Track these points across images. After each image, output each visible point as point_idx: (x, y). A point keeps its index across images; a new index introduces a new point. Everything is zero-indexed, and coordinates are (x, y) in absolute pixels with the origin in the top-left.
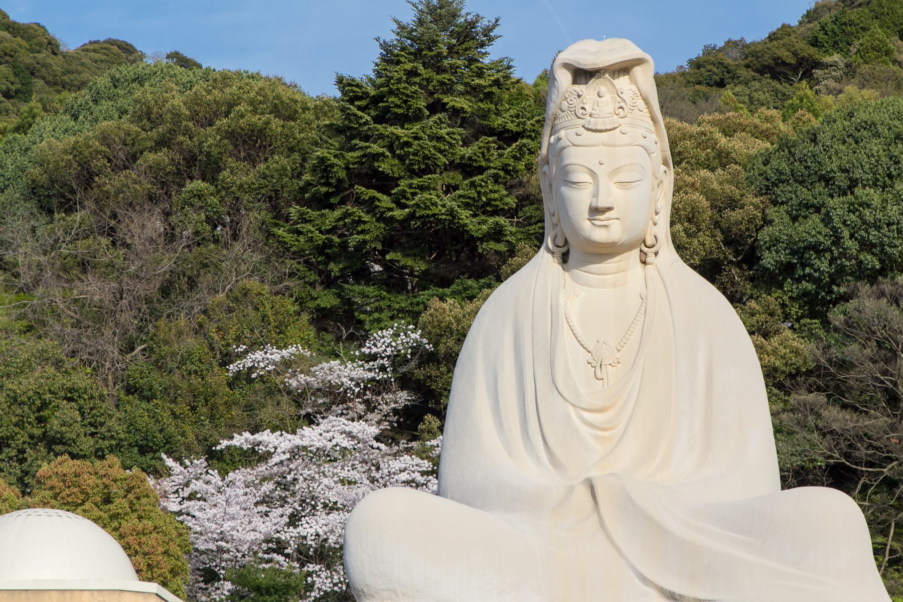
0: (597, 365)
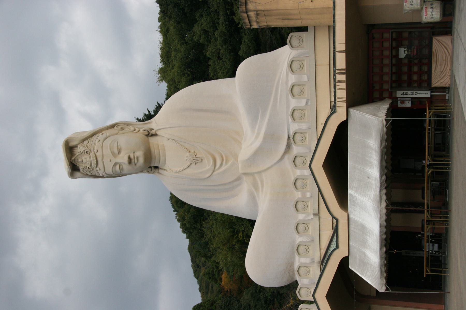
0: (197, 161)
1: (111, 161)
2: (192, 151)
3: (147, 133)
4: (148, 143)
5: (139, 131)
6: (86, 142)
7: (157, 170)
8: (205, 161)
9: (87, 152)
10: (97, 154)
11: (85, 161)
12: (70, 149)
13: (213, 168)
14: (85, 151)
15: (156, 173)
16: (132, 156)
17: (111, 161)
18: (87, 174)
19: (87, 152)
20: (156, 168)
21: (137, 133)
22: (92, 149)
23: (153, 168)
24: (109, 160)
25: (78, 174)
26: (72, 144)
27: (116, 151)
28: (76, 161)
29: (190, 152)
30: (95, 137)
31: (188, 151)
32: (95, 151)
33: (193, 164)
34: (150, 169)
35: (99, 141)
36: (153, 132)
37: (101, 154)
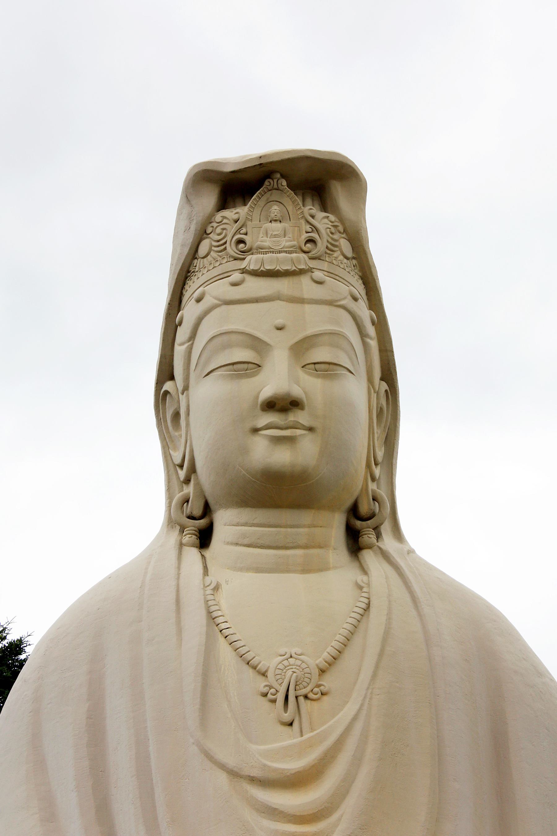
1: (280, 329)
2: (328, 682)
3: (364, 509)
4: (331, 508)
5: (373, 479)
6: (345, 246)
7: (189, 538)
8: (290, 739)
9: (311, 241)
10: (305, 280)
11: (274, 227)
12: (319, 180)
13: (255, 773)
14: (315, 235)
15: (174, 535)
16: (299, 417)
17: (280, 329)
18: (202, 234)
19: (311, 241)
20: (204, 538)
21: (368, 466)
22: (325, 266)
23: (202, 523)
24: (279, 322)
25: (209, 199)
26: (339, 193)
27: (321, 354)
28: (275, 195)
29: (322, 671)
30: (359, 289)
31: (324, 665)
32: (317, 275)
33: (261, 684)
34: (198, 512)
35: (355, 299)
36: (369, 537)
37: (306, 295)
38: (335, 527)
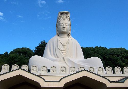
3: (69, 34)
38: (67, 35)
